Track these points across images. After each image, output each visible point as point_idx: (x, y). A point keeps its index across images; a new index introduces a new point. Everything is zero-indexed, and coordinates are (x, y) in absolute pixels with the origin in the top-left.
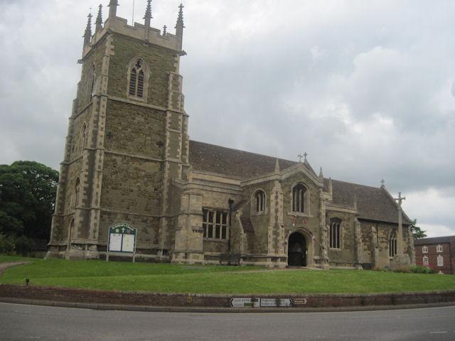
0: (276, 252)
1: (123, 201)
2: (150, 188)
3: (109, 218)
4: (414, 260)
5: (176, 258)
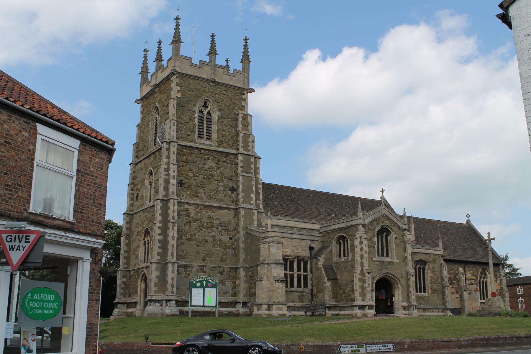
0: (363, 300)
1: (198, 252)
2: (225, 238)
3: (185, 271)
4: (508, 302)
5: (258, 310)
